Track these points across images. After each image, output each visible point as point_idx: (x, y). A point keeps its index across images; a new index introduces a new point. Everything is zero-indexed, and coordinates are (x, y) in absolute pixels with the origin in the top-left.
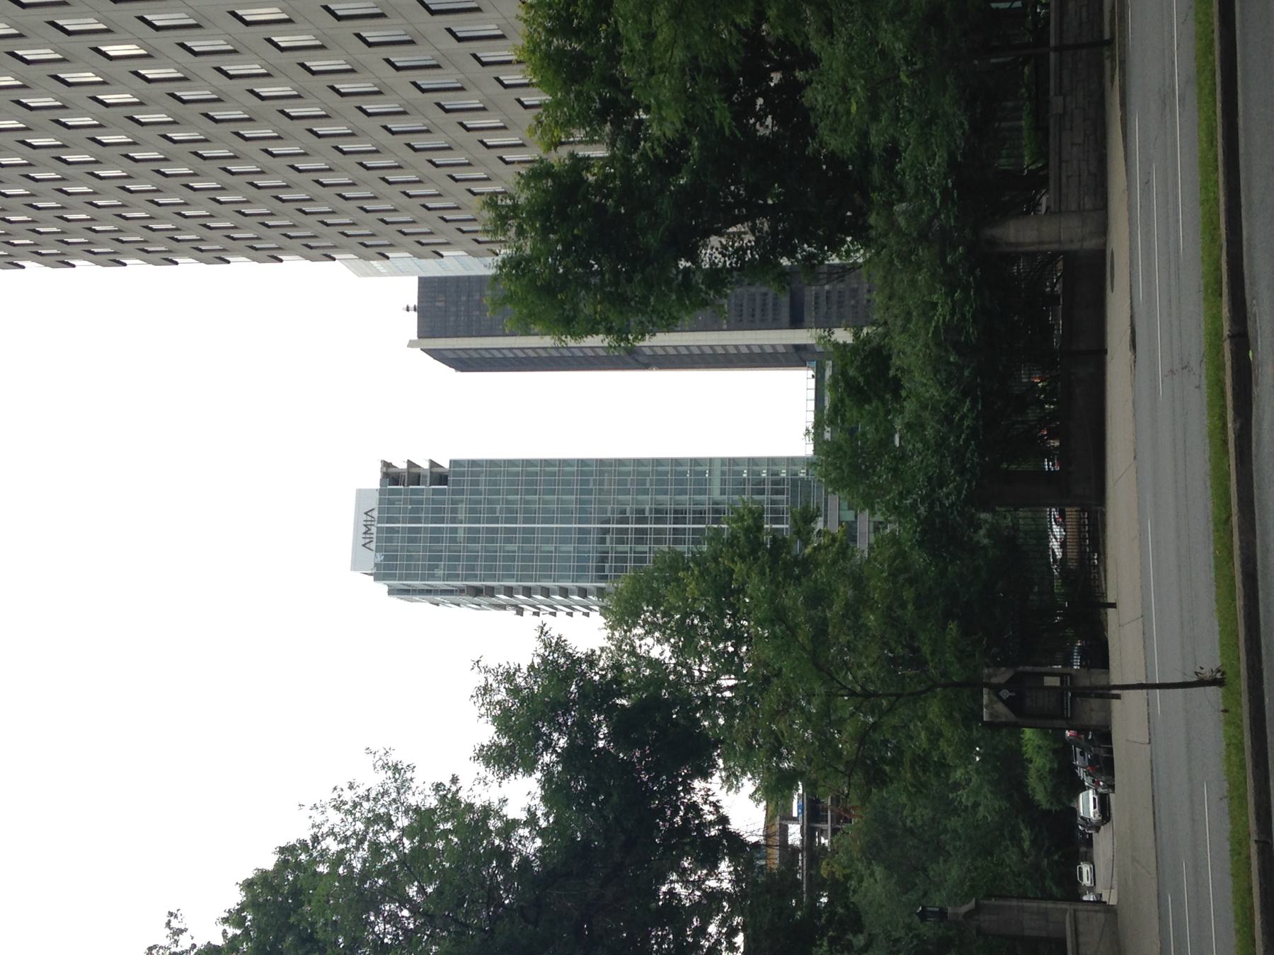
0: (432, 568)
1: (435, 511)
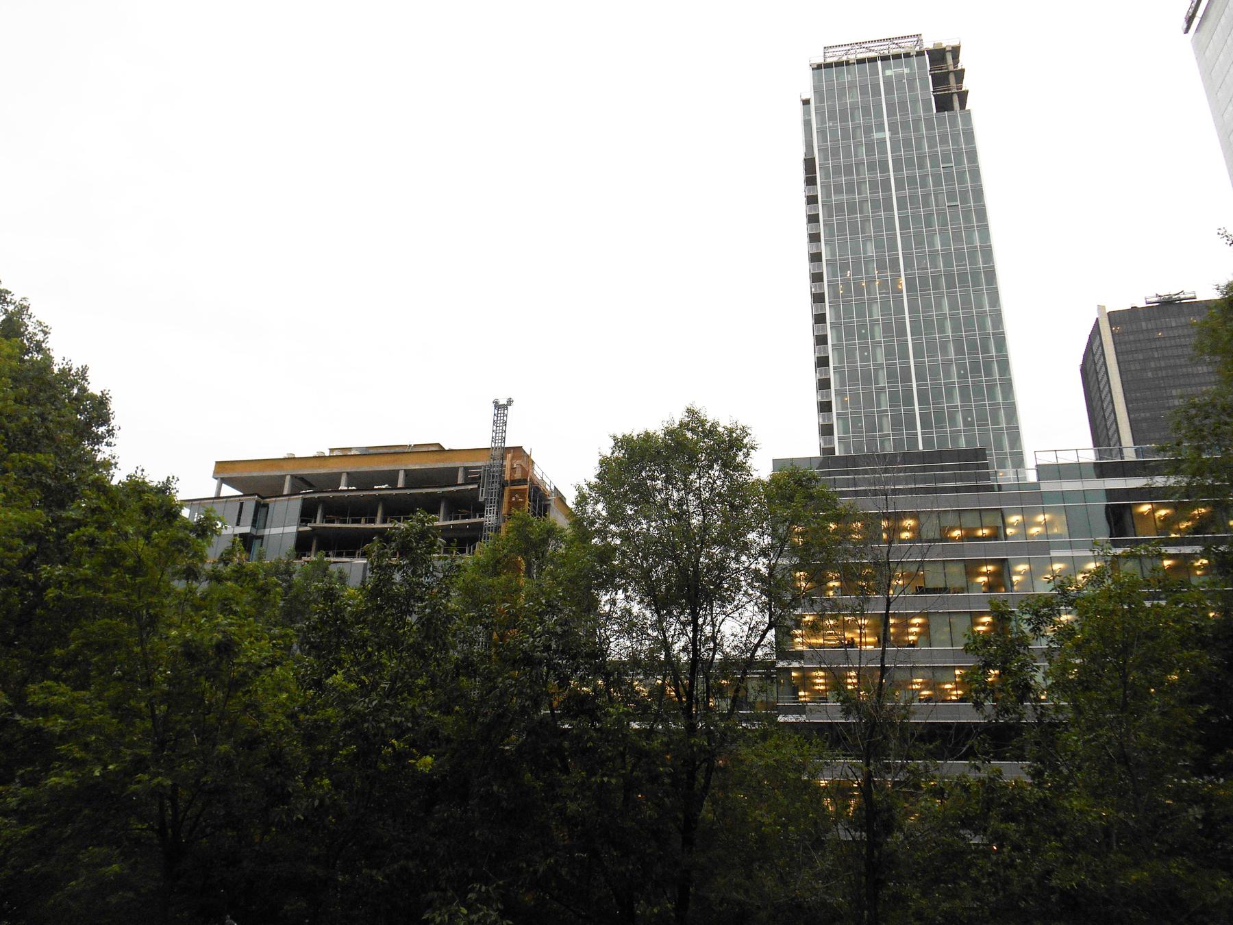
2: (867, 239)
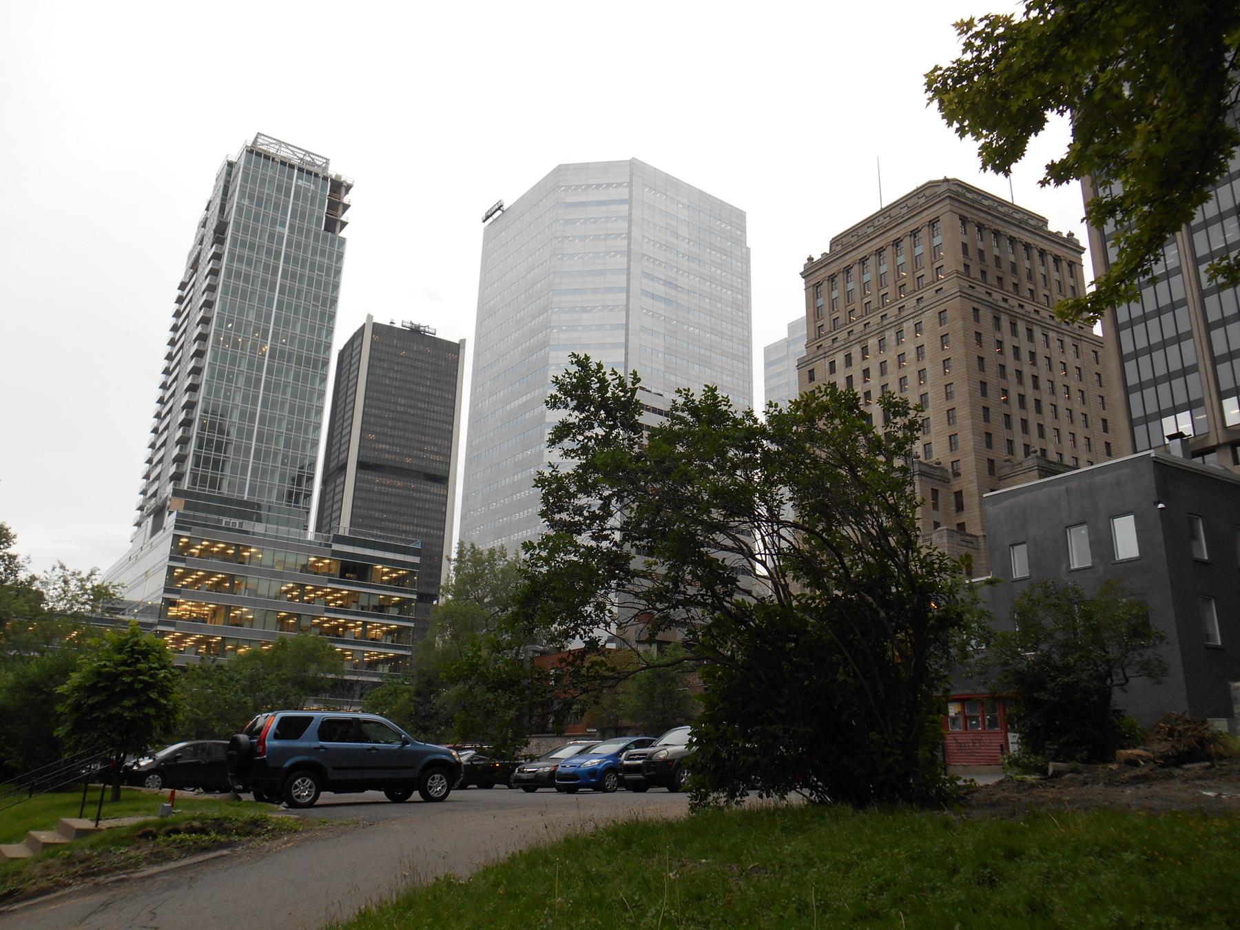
0: (251, 197)
1: (303, 214)
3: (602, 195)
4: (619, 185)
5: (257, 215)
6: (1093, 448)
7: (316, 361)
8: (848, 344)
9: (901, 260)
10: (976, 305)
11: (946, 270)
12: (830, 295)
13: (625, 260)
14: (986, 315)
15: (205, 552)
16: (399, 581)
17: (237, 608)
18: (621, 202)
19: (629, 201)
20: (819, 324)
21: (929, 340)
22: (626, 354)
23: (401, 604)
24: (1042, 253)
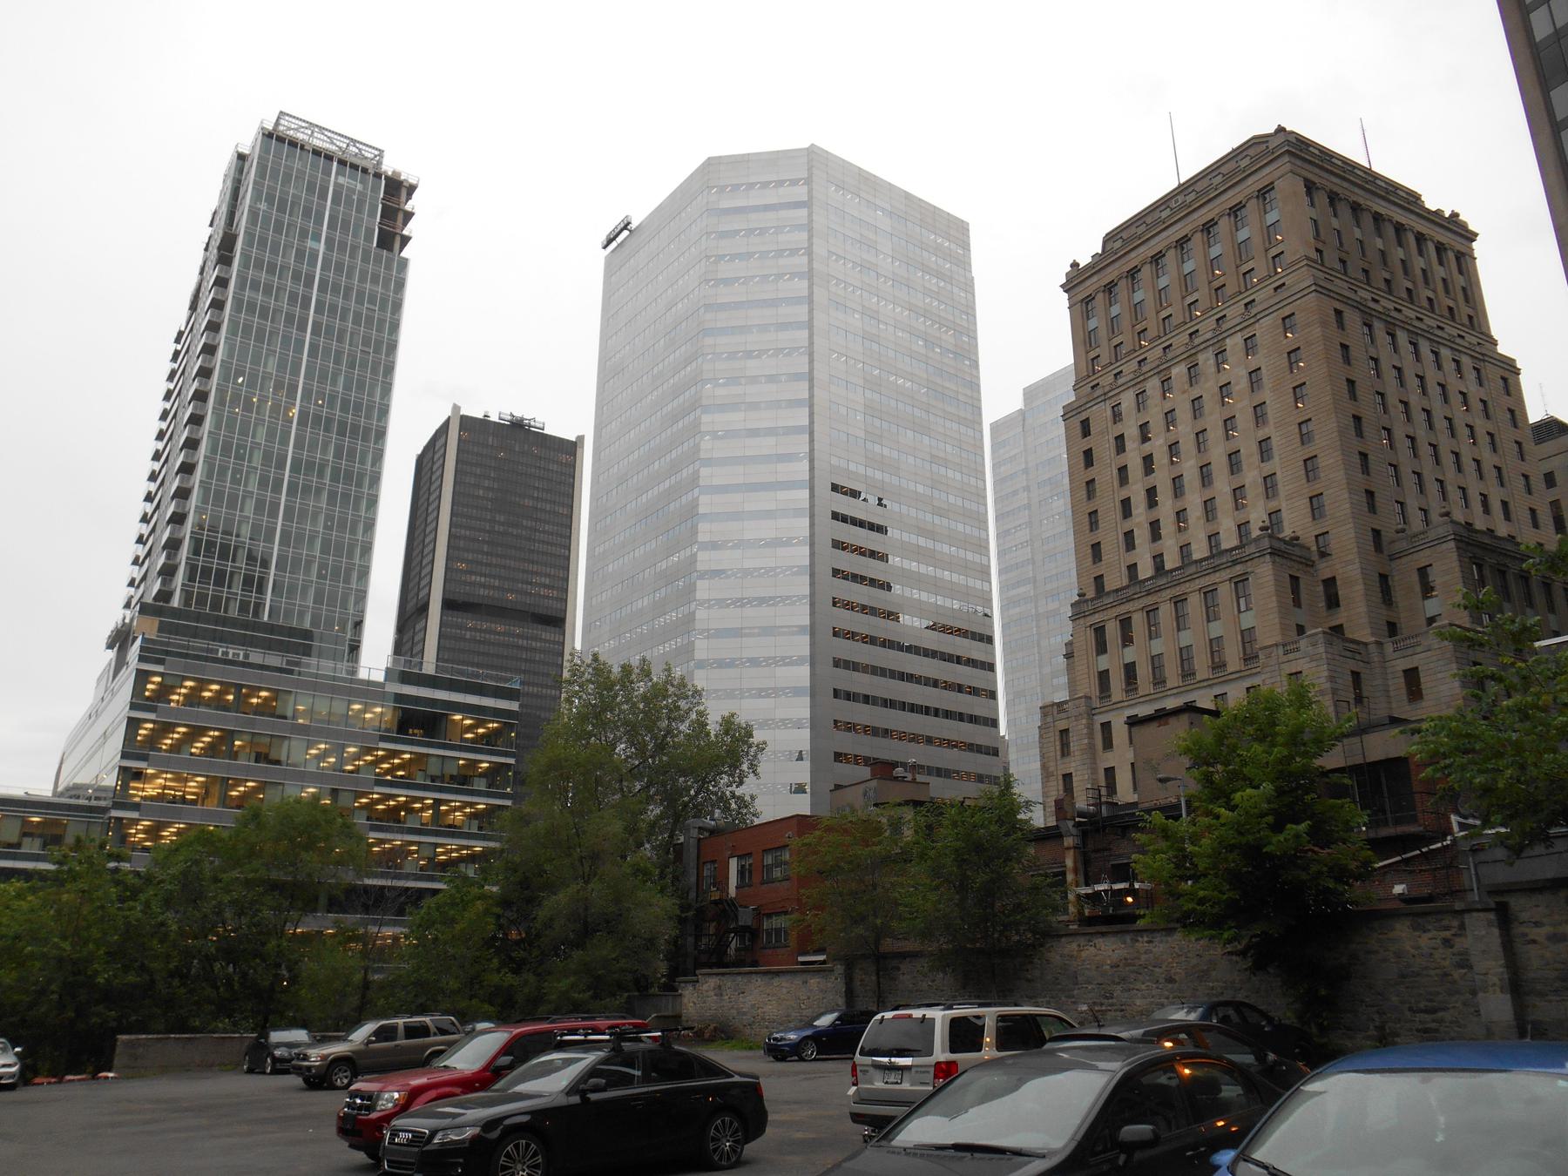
0: (270, 200)
2: (271, 352)
3: (771, 197)
4: (794, 182)
5: (279, 224)
6: (1513, 516)
7: (367, 430)
8: (1139, 379)
9: (1215, 251)
10: (1339, 306)
11: (1288, 258)
12: (1107, 311)
13: (805, 283)
14: (1352, 318)
15: (193, 699)
16: (489, 740)
17: (239, 782)
18: (797, 205)
19: (807, 204)
20: (1092, 354)
21: (1268, 360)
22: (811, 415)
23: (497, 769)
24: (1420, 238)
